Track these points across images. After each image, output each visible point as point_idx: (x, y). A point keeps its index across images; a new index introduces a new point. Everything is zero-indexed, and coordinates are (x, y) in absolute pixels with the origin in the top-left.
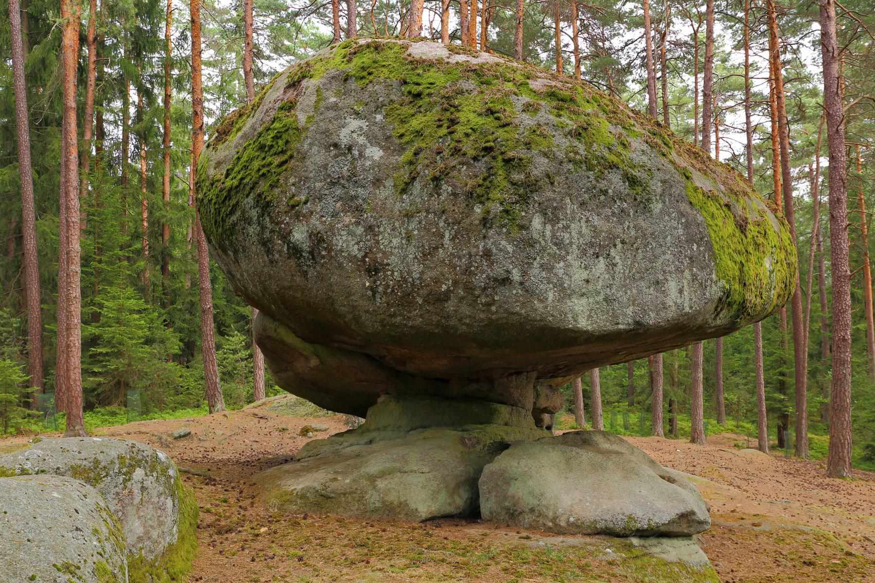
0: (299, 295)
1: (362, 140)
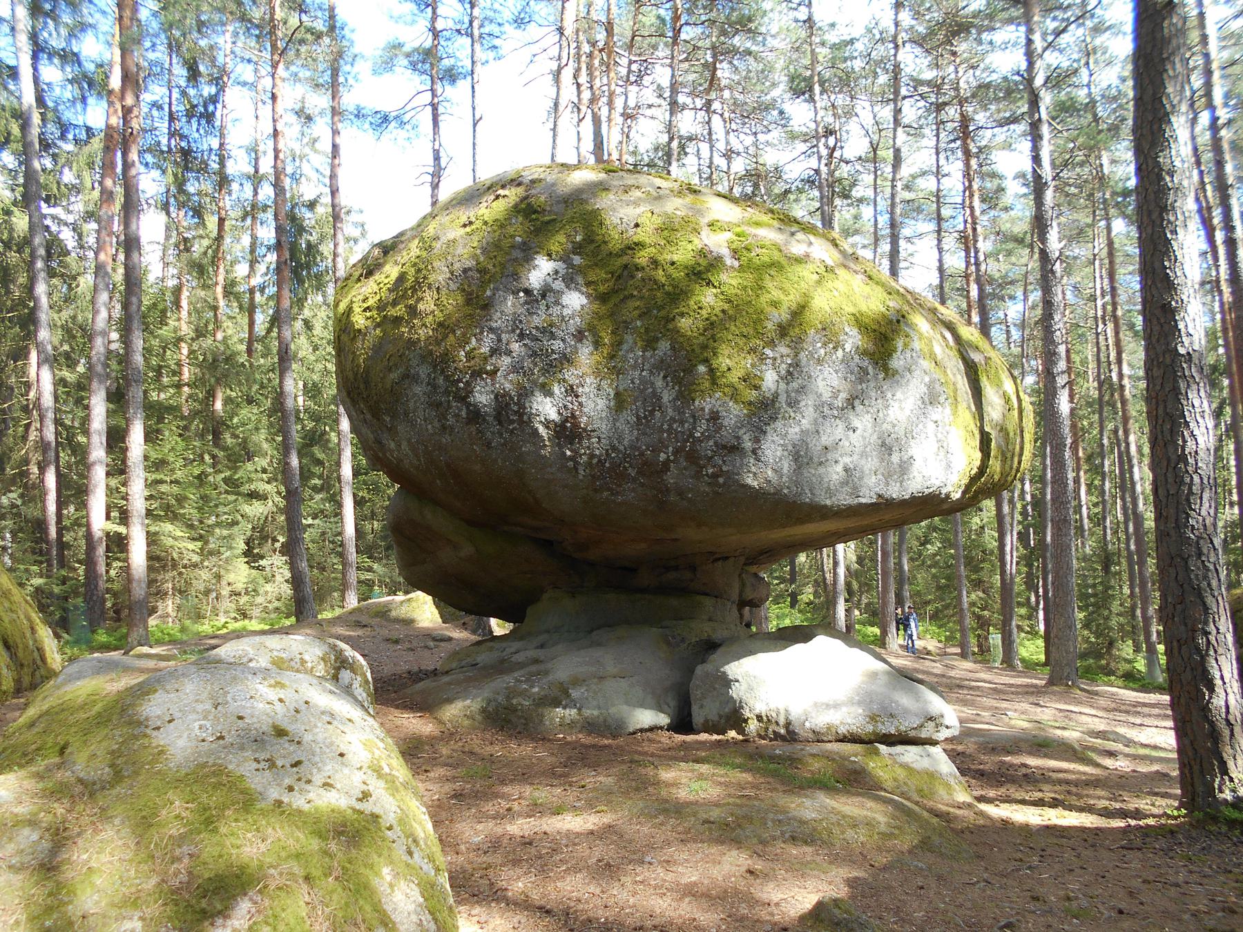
0: (477, 467)
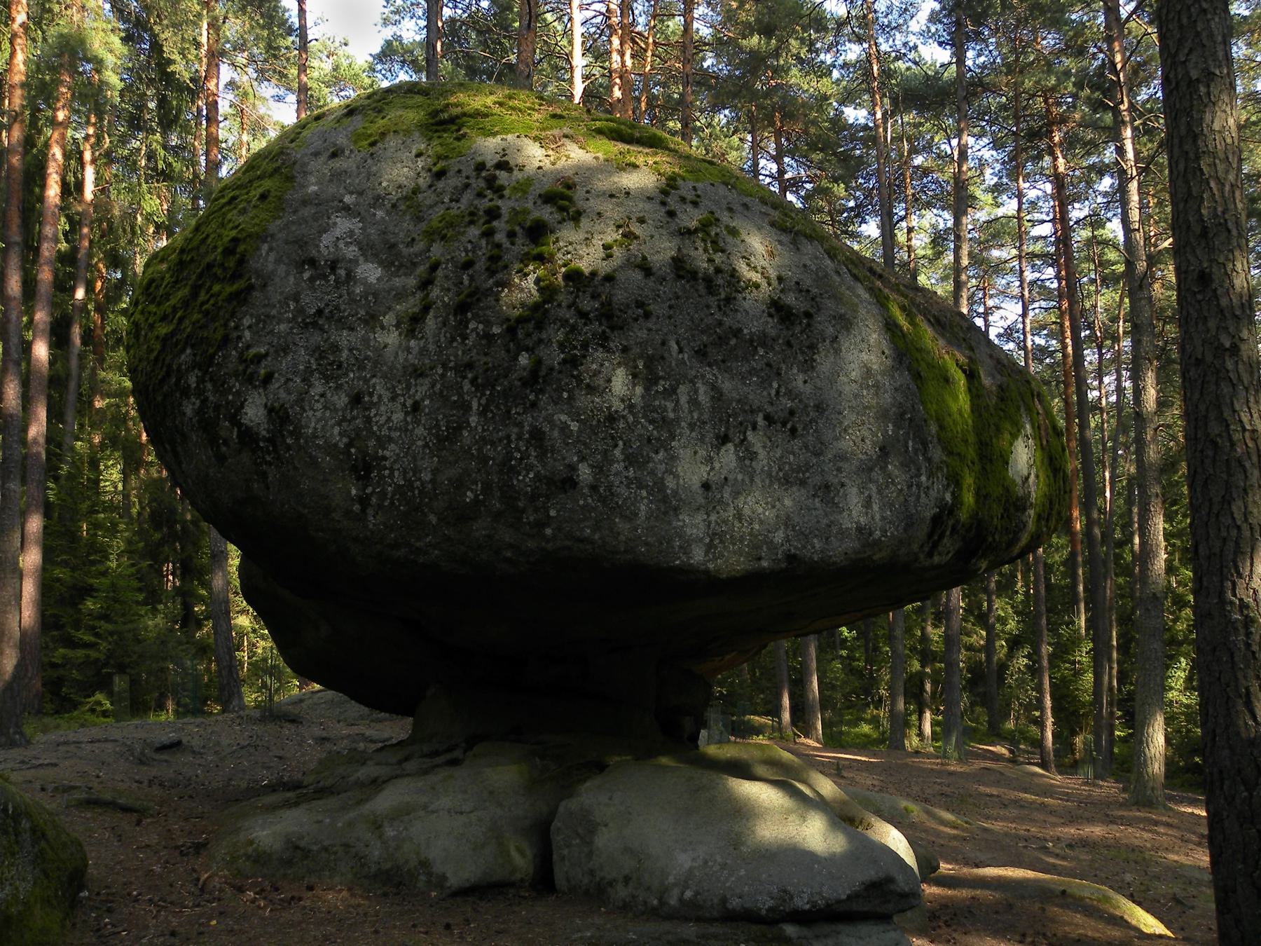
1: (351, 252)
